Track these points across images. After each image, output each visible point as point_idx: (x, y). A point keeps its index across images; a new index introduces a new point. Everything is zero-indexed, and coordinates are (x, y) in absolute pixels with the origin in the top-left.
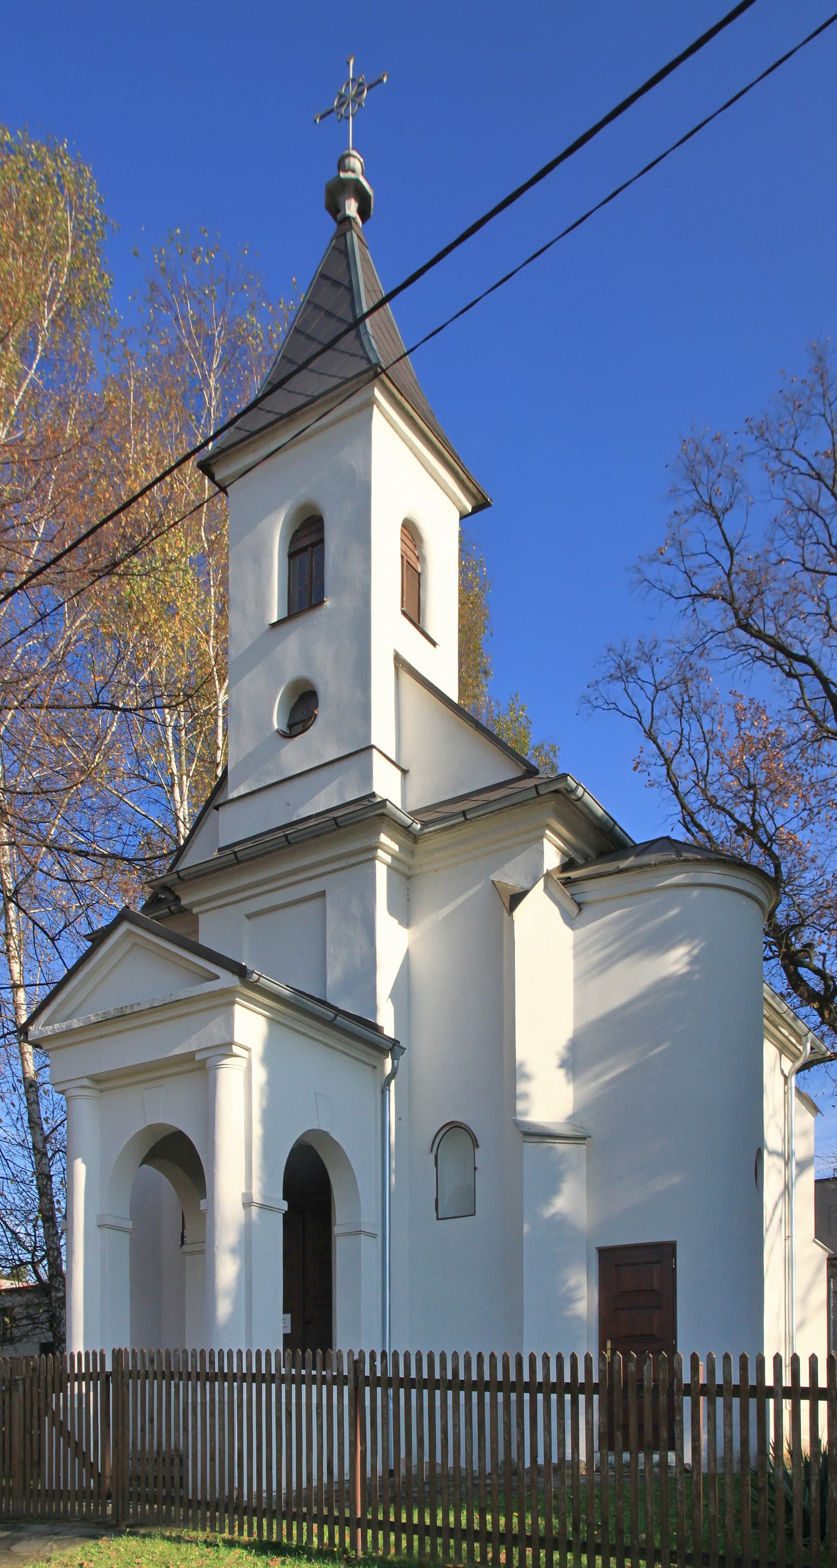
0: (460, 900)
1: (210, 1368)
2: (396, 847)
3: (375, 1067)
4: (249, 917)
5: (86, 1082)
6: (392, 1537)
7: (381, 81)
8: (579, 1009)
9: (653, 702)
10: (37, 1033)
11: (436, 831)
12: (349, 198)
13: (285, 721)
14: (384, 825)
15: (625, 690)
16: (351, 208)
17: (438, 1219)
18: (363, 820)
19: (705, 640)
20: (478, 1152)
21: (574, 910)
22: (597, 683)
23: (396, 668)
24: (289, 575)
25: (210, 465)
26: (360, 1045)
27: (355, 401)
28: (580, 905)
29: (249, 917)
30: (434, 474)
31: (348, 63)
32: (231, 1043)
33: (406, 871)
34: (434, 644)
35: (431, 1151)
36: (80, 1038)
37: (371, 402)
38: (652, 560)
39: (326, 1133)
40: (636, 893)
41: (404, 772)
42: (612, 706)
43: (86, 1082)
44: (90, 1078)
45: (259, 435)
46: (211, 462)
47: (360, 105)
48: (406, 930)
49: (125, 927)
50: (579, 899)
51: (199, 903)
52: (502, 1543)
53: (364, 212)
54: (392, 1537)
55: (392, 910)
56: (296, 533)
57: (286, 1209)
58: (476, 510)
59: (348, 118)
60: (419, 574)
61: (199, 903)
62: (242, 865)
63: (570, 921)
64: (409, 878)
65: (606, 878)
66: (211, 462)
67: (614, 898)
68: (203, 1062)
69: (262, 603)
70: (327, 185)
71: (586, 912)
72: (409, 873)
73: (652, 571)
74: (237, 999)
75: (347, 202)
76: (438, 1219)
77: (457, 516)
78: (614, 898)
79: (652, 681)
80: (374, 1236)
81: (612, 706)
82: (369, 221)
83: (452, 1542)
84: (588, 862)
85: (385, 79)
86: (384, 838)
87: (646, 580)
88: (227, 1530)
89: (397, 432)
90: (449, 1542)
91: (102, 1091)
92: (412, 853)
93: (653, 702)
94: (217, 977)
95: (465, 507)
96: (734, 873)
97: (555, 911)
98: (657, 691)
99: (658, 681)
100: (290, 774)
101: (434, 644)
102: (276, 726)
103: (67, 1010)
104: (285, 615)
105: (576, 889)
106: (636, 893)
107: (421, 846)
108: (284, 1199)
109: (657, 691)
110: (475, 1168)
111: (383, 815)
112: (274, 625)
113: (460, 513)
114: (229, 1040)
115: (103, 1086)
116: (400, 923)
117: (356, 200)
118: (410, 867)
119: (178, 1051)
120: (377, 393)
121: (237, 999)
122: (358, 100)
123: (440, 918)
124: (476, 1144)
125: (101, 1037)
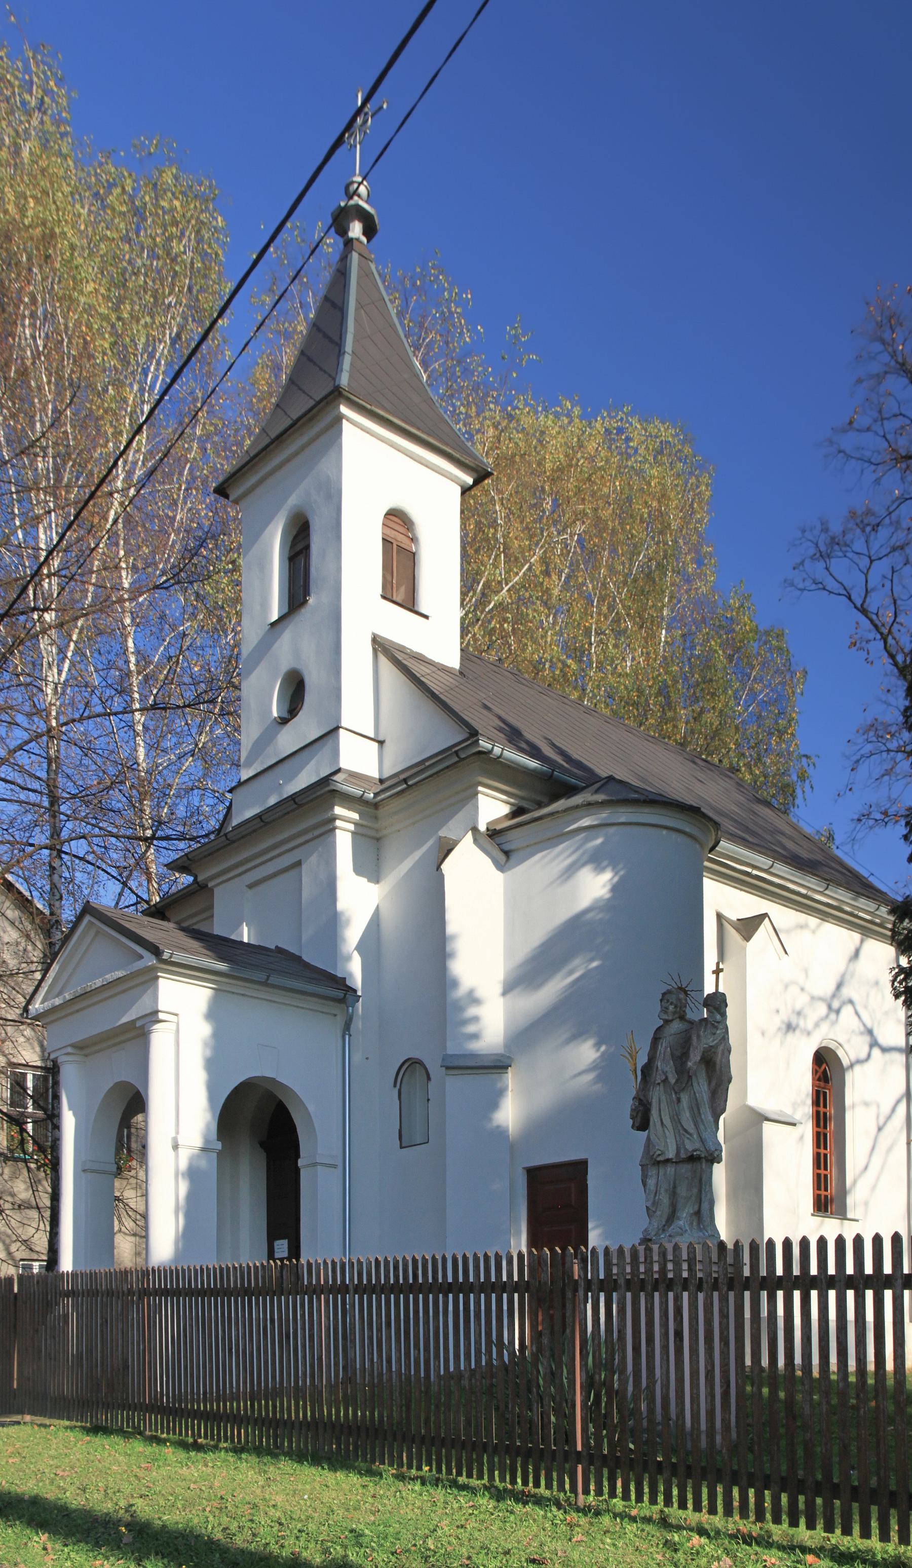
0: (417, 855)
1: (625, 1298)
2: (356, 816)
3: (335, 1015)
4: (251, 886)
5: (69, 1050)
6: (784, 1499)
7: (381, 108)
8: (509, 949)
9: (866, 575)
10: (34, 1011)
11: (390, 797)
12: (353, 220)
13: (286, 707)
14: (336, 799)
15: (827, 569)
16: (356, 230)
17: (401, 1147)
18: (312, 801)
19: (891, 509)
20: (431, 1085)
21: (502, 857)
22: (802, 563)
23: (375, 651)
24: (290, 576)
25: (224, 489)
26: (309, 998)
27: (328, 419)
28: (507, 854)
29: (251, 886)
30: (423, 461)
31: (357, 96)
32: (157, 1012)
33: (373, 833)
34: (426, 617)
35: (395, 1086)
36: (64, 1013)
37: (340, 418)
38: (844, 431)
39: (274, 1079)
40: (553, 838)
41: (381, 743)
42: (821, 586)
43: (69, 1050)
44: (73, 1046)
45: (257, 459)
46: (225, 486)
47: (365, 133)
48: (372, 885)
49: (87, 918)
50: (507, 847)
51: (213, 878)
52: (893, 1504)
53: (370, 231)
54: (784, 1499)
55: (359, 869)
56: (295, 537)
57: (220, 1148)
58: (477, 482)
59: (356, 147)
60: (414, 554)
61: (213, 878)
62: (235, 845)
63: (501, 867)
64: (378, 839)
65: (526, 827)
66: (225, 486)
67: (535, 844)
68: (143, 1027)
69: (265, 606)
70: (332, 214)
71: (514, 858)
72: (378, 836)
73: (848, 441)
74: (159, 974)
75: (351, 225)
76: (401, 1147)
77: (458, 490)
78: (535, 844)
79: (867, 553)
80: (335, 1166)
81: (821, 586)
82: (375, 240)
83: (819, 1501)
84: (540, 805)
85: (385, 106)
86: (338, 810)
87: (840, 452)
88: (486, 1477)
89: (372, 435)
90: (814, 1501)
91: (86, 1056)
92: (376, 818)
93: (866, 575)
94: (141, 957)
95: (465, 482)
96: (647, 810)
97: (487, 861)
98: (871, 562)
99: (872, 554)
100: (286, 755)
101: (426, 617)
102: (275, 714)
103: (57, 989)
104: (286, 610)
105: (500, 839)
106: (553, 838)
107: (382, 812)
108: (218, 1140)
109: (871, 562)
110: (428, 1100)
111: (334, 790)
112: (273, 625)
113: (462, 487)
114: (155, 1009)
115: (87, 1051)
116: (369, 881)
117: (359, 221)
118: (377, 830)
119: (124, 1020)
120: (344, 409)
121: (159, 974)
122: (363, 129)
123: (402, 874)
124: (429, 1078)
125: (78, 1011)
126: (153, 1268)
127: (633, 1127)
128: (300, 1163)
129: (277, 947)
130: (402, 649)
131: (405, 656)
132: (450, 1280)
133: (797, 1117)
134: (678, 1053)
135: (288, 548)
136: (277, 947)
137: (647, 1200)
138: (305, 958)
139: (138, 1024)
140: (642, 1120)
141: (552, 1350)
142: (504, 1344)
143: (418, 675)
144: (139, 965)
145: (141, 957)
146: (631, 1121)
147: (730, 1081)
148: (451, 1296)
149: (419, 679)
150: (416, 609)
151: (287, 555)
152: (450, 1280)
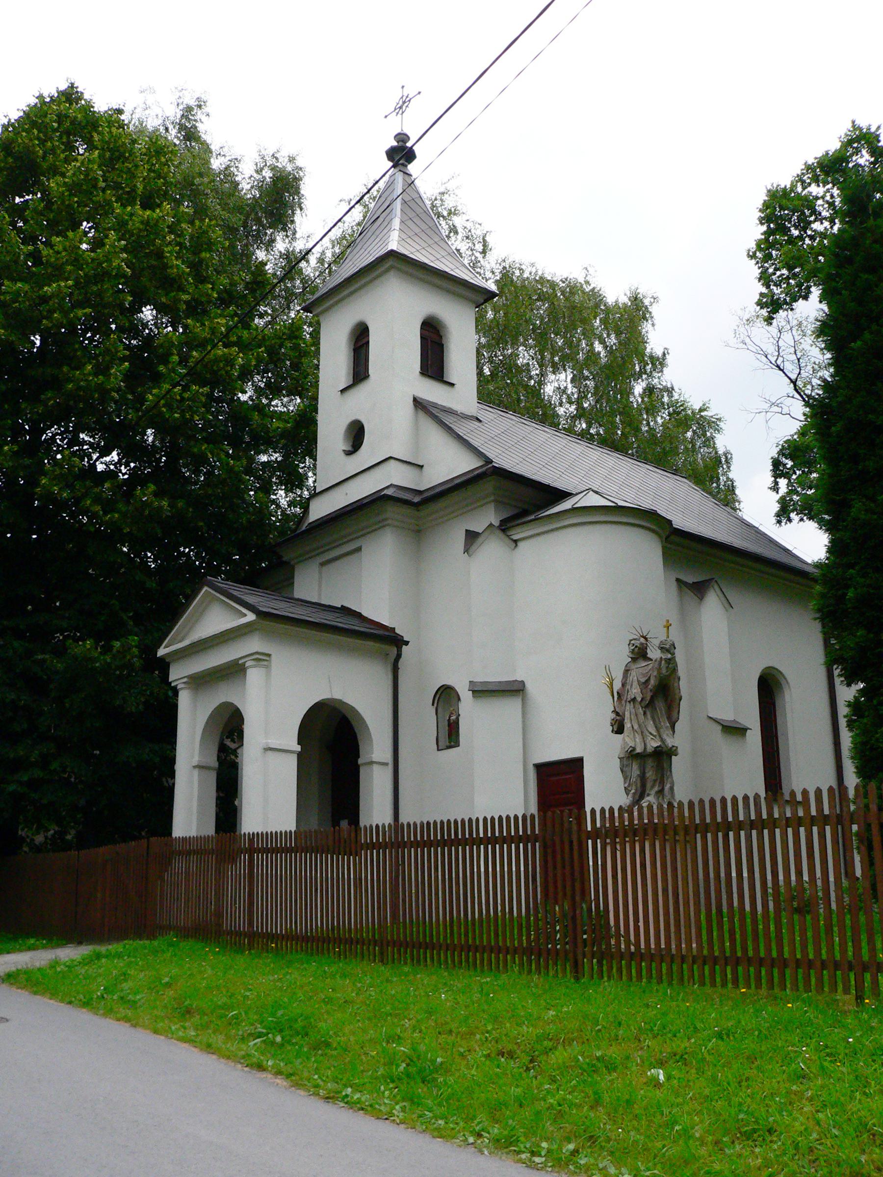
17: (438, 750)
57: (299, 750)
76: (438, 750)
94: (245, 615)
101: (452, 385)
126: (245, 834)
127: (612, 732)
128: (360, 761)
129: (342, 606)
130: (435, 405)
131: (438, 411)
132: (481, 835)
133: (744, 722)
134: (643, 680)
135: (353, 343)
136: (342, 606)
137: (625, 783)
138: (365, 614)
139: (240, 662)
140: (619, 728)
141: (856, 986)
142: (620, 934)
143: (448, 423)
144: (244, 620)
145: (245, 615)
146: (611, 728)
147: (680, 699)
148: (482, 847)
149: (447, 425)
150: (445, 379)
151: (352, 347)
152: (481, 835)
